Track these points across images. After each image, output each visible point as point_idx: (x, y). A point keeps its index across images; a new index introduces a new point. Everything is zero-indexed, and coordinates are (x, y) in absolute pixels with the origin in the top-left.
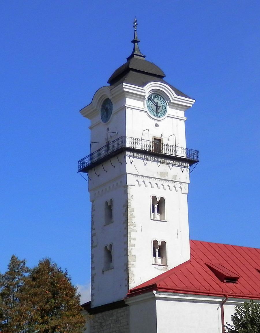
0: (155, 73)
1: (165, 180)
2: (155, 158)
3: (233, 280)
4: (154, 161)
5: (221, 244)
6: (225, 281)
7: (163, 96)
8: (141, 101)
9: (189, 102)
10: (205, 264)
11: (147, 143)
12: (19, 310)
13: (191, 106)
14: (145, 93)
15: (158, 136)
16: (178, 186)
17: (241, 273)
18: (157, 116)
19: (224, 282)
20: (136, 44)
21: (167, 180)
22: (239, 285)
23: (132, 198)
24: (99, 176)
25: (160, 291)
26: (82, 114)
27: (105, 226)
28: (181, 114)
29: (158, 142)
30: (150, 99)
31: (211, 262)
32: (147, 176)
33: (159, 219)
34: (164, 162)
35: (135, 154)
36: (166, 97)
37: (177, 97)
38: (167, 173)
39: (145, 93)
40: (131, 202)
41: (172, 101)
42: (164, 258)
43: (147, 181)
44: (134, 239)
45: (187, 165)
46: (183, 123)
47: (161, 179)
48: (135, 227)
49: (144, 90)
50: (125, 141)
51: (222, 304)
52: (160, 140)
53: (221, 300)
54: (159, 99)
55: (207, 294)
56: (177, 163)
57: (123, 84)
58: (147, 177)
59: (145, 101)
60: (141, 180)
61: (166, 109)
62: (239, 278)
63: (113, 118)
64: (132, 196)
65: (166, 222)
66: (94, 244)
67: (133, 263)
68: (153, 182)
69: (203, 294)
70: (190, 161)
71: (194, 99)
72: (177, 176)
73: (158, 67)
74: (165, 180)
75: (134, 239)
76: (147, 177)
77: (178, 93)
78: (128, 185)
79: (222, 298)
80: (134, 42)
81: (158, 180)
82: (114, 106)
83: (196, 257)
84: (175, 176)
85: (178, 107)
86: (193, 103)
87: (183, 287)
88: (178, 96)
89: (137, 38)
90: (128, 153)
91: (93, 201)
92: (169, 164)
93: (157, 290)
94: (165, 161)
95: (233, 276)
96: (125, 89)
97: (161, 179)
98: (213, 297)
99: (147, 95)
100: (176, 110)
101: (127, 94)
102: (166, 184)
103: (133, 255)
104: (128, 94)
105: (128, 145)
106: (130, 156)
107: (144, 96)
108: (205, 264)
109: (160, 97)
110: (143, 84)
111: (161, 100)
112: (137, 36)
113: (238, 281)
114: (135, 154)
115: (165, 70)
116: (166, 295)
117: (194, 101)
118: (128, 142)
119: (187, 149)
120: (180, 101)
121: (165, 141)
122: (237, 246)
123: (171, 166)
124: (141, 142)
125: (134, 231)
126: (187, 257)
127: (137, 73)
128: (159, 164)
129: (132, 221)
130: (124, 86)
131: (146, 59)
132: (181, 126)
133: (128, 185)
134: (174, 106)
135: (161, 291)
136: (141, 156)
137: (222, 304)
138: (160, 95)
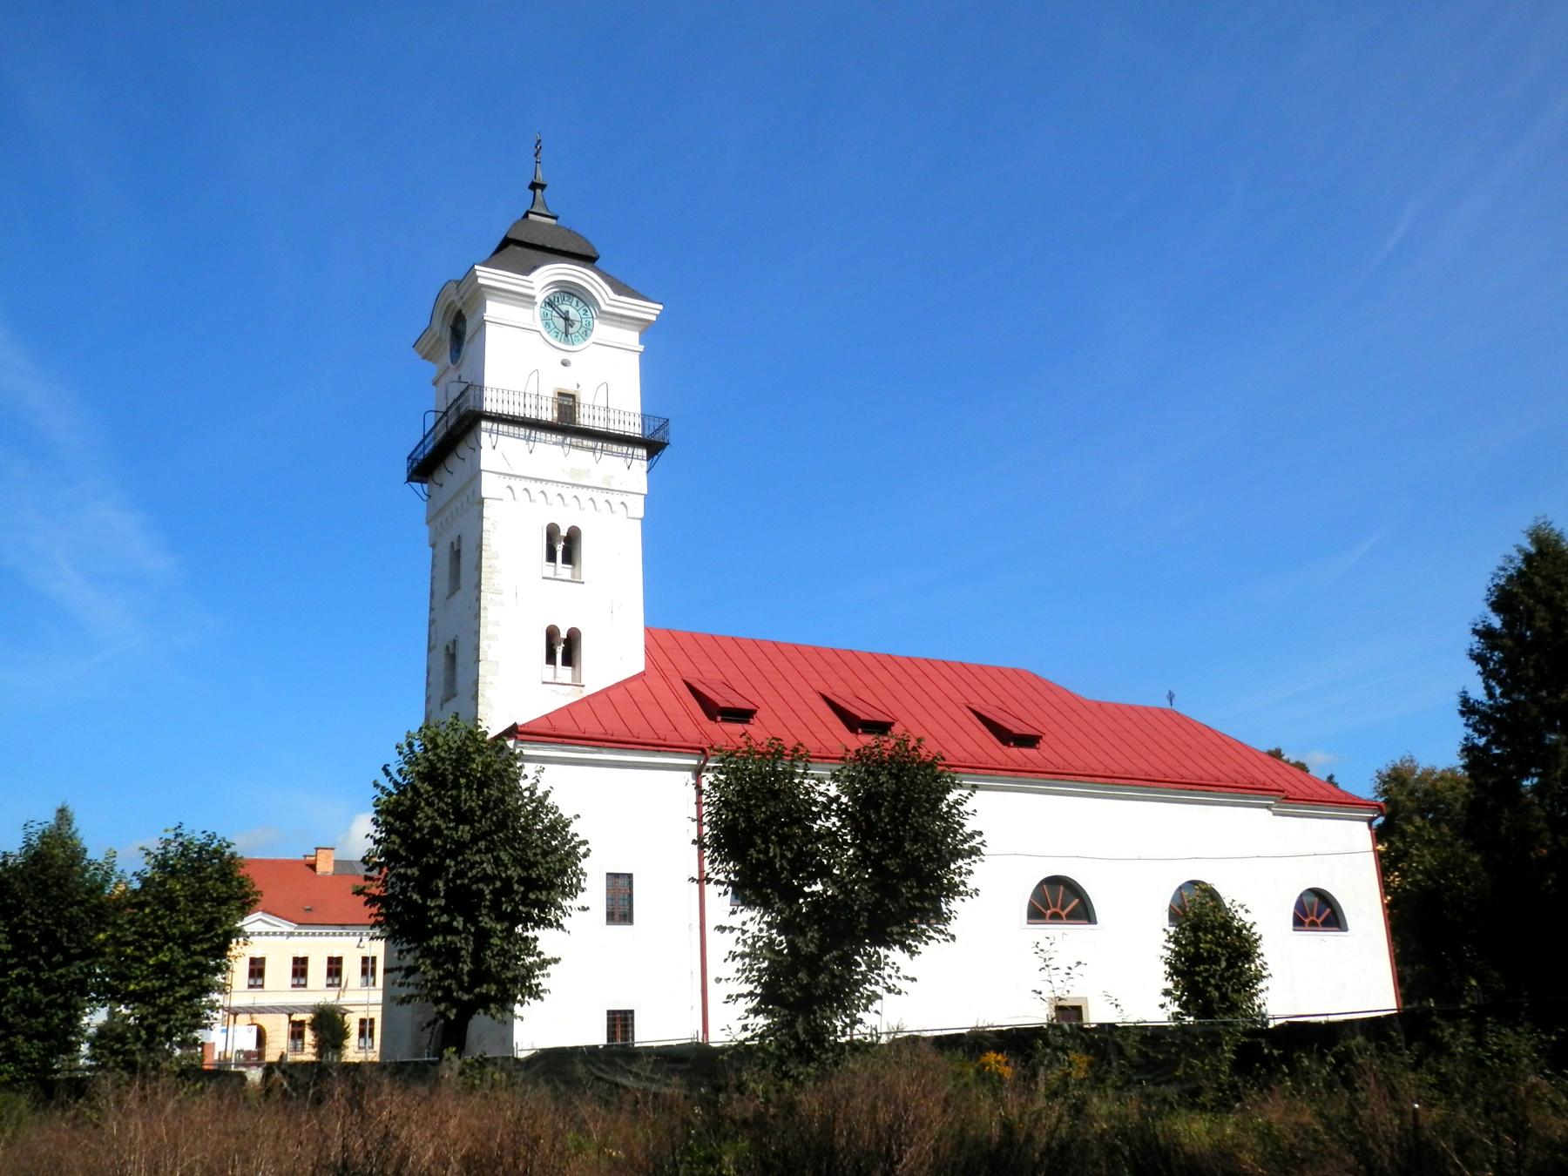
0: (572, 250)
1: (583, 487)
2: (559, 437)
3: (1029, 741)
4: (554, 443)
5: (973, 665)
6: (719, 718)
7: (583, 298)
8: (528, 308)
9: (649, 311)
10: (684, 681)
13: (654, 318)
14: (533, 288)
15: (569, 388)
16: (615, 499)
17: (757, 700)
18: (567, 342)
19: (716, 722)
20: (539, 191)
21: (588, 487)
24: (441, 485)
25: (523, 741)
26: (420, 353)
27: (448, 598)
28: (632, 338)
29: (567, 403)
30: (550, 303)
31: (1000, 705)
33: (569, 578)
34: (609, 449)
35: (533, 432)
39: (533, 288)
41: (604, 308)
42: (577, 669)
43: (535, 488)
44: (497, 624)
45: (642, 452)
46: (636, 357)
50: (481, 399)
52: (573, 397)
53: (695, 762)
54: (574, 303)
55: (656, 748)
56: (615, 448)
58: (536, 480)
59: (537, 308)
60: (518, 485)
61: (591, 327)
62: (892, 724)
63: (468, 349)
66: (432, 644)
67: (489, 679)
68: (552, 490)
69: (628, 746)
70: (653, 446)
72: (613, 477)
73: (583, 238)
74: (583, 487)
75: (497, 624)
76: (536, 480)
77: (620, 288)
79: (697, 756)
80: (534, 186)
82: (468, 324)
83: (665, 664)
85: (621, 322)
86: (658, 312)
87: (648, 737)
88: (620, 295)
89: (540, 179)
90: (485, 424)
91: (433, 546)
92: (594, 450)
93: (516, 738)
94: (585, 442)
95: (738, 706)
96: (480, 281)
98: (671, 754)
99: (540, 297)
102: (584, 495)
104: (491, 291)
105: (489, 406)
106: (491, 431)
107: (533, 297)
108: (684, 681)
109: (575, 299)
110: (527, 270)
112: (539, 174)
114: (501, 427)
115: (599, 246)
116: (543, 749)
117: (661, 307)
118: (489, 400)
119: (644, 416)
121: (585, 398)
122: (992, 667)
123: (598, 455)
124: (522, 399)
126: (633, 662)
127: (525, 250)
128: (566, 449)
129: (493, 582)
130: (478, 273)
131: (561, 222)
136: (522, 431)
138: (574, 295)
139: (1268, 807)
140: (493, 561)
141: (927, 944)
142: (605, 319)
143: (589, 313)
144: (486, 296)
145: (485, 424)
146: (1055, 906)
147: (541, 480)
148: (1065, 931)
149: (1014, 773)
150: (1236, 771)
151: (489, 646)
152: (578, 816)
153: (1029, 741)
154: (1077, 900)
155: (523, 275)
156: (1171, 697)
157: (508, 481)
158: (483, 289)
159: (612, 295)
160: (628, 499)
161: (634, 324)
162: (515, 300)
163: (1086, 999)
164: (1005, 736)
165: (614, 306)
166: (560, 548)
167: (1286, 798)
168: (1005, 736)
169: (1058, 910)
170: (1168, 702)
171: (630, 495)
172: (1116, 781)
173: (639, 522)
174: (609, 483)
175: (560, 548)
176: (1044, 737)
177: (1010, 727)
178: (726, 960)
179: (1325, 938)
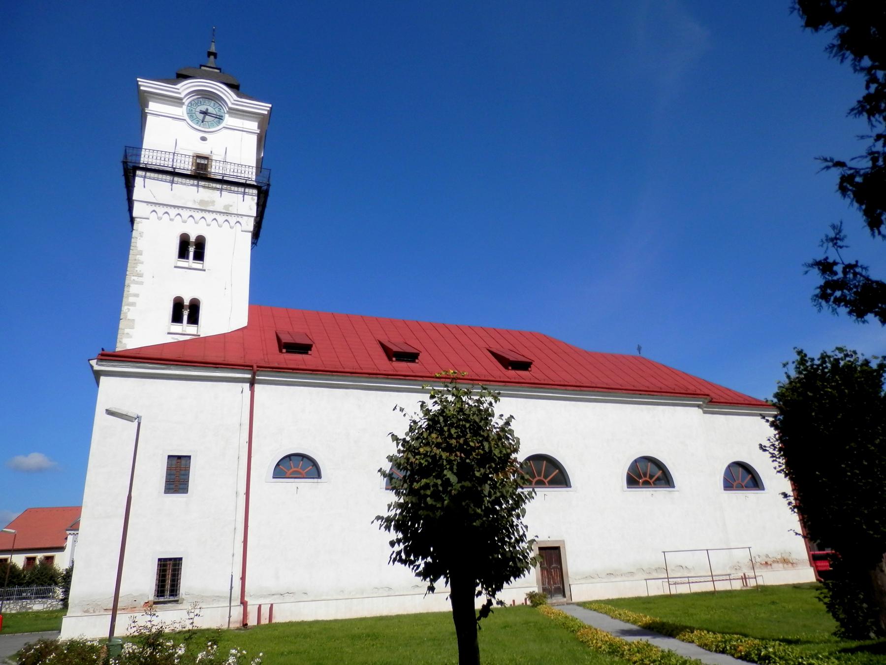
1: (209, 211)
9: (264, 108)
11: (171, 157)
12: (440, 412)
13: (266, 113)
14: (180, 93)
16: (233, 220)
22: (420, 365)
23: (141, 236)
32: (262, 231)
36: (213, 95)
44: (137, 295)
47: (202, 210)
48: (140, 278)
49: (178, 89)
51: (252, 383)
57: (138, 79)
58: (175, 207)
60: (161, 210)
64: (141, 234)
68: (185, 214)
74: (209, 211)
75: (137, 295)
76: (175, 207)
78: (137, 218)
84: (227, 207)
85: (243, 115)
86: (269, 109)
88: (241, 98)
90: (139, 173)
96: (142, 88)
97: (202, 210)
100: (242, 120)
101: (153, 97)
108: (276, 333)
109: (213, 102)
111: (214, 106)
116: (119, 366)
117: (270, 106)
126: (241, 321)
129: (136, 269)
132: (252, 141)
133: (137, 218)
135: (738, 404)
137: (252, 383)
139: (699, 406)
140: (138, 256)
143: (222, 110)
144: (148, 98)
145: (139, 173)
146: (539, 475)
147: (178, 207)
148: (546, 493)
149: (504, 384)
150: (676, 385)
151: (129, 310)
152: (789, 531)
153: (524, 366)
154: (557, 471)
155: (173, 85)
156: (639, 349)
157: (153, 208)
158: (146, 94)
160: (243, 220)
161: (256, 117)
162: (168, 101)
163: (563, 541)
164: (506, 363)
167: (711, 402)
168: (506, 363)
169: (542, 478)
170: (638, 353)
171: (244, 217)
172: (582, 388)
176: (533, 363)
177: (507, 357)
178: (373, 522)
179: (748, 495)
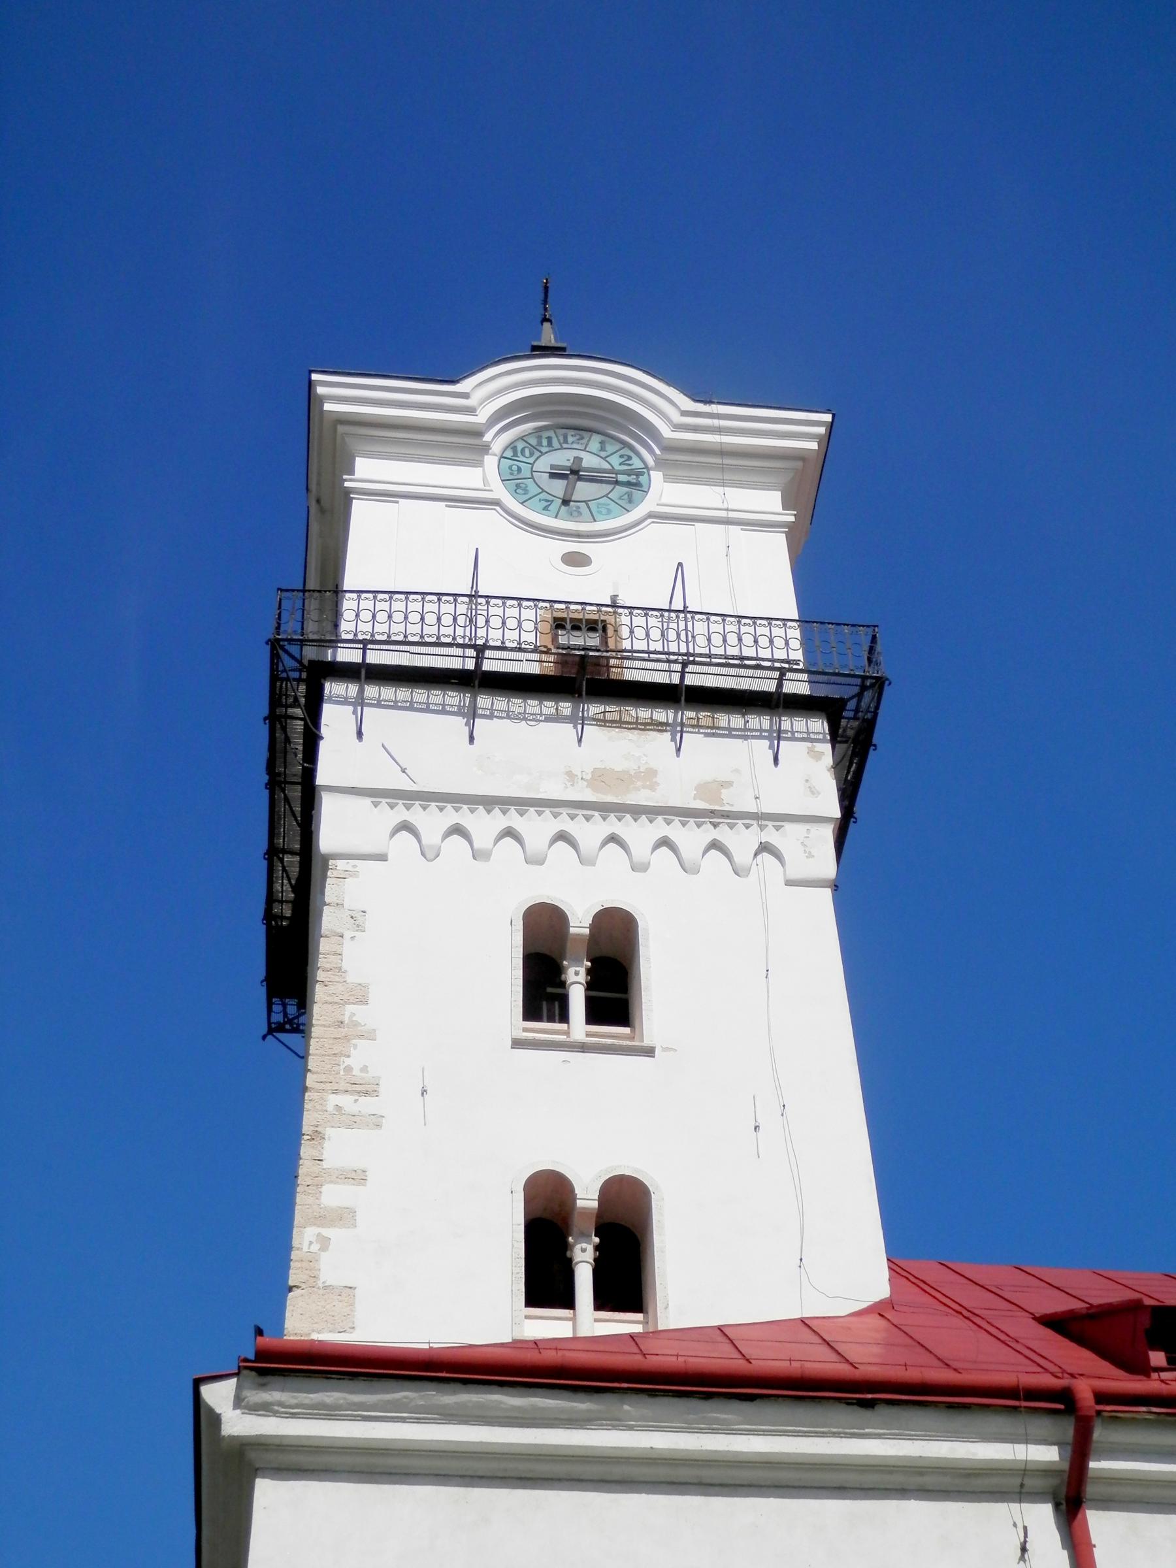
4: (549, 719)
14: (471, 410)
16: (742, 841)
23: (360, 928)
37: (701, 407)
38: (652, 773)
40: (348, 948)
42: (1027, 1563)
44: (357, 1177)
46: (778, 544)
60: (432, 822)
64: (357, 920)
65: (649, 1052)
71: (828, 411)
75: (357, 1177)
81: (580, 812)
83: (930, 1272)
85: (723, 468)
103: (325, 1288)
113: (331, 684)
117: (828, 418)
120: (719, 430)
125: (353, 1121)
130: (320, 390)
134: (689, 466)
136: (454, 698)
140: (350, 1008)
141: (428, 854)
142: (676, 464)
151: (325, 1242)
158: (341, 429)
159: (687, 404)
160: (787, 839)
165: (696, 429)
166: (576, 979)
173: (827, 893)
174: (720, 801)
175: (576, 979)
